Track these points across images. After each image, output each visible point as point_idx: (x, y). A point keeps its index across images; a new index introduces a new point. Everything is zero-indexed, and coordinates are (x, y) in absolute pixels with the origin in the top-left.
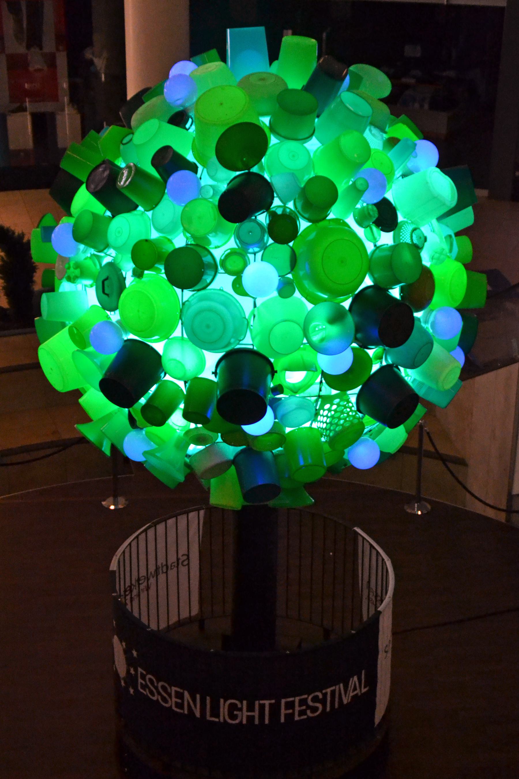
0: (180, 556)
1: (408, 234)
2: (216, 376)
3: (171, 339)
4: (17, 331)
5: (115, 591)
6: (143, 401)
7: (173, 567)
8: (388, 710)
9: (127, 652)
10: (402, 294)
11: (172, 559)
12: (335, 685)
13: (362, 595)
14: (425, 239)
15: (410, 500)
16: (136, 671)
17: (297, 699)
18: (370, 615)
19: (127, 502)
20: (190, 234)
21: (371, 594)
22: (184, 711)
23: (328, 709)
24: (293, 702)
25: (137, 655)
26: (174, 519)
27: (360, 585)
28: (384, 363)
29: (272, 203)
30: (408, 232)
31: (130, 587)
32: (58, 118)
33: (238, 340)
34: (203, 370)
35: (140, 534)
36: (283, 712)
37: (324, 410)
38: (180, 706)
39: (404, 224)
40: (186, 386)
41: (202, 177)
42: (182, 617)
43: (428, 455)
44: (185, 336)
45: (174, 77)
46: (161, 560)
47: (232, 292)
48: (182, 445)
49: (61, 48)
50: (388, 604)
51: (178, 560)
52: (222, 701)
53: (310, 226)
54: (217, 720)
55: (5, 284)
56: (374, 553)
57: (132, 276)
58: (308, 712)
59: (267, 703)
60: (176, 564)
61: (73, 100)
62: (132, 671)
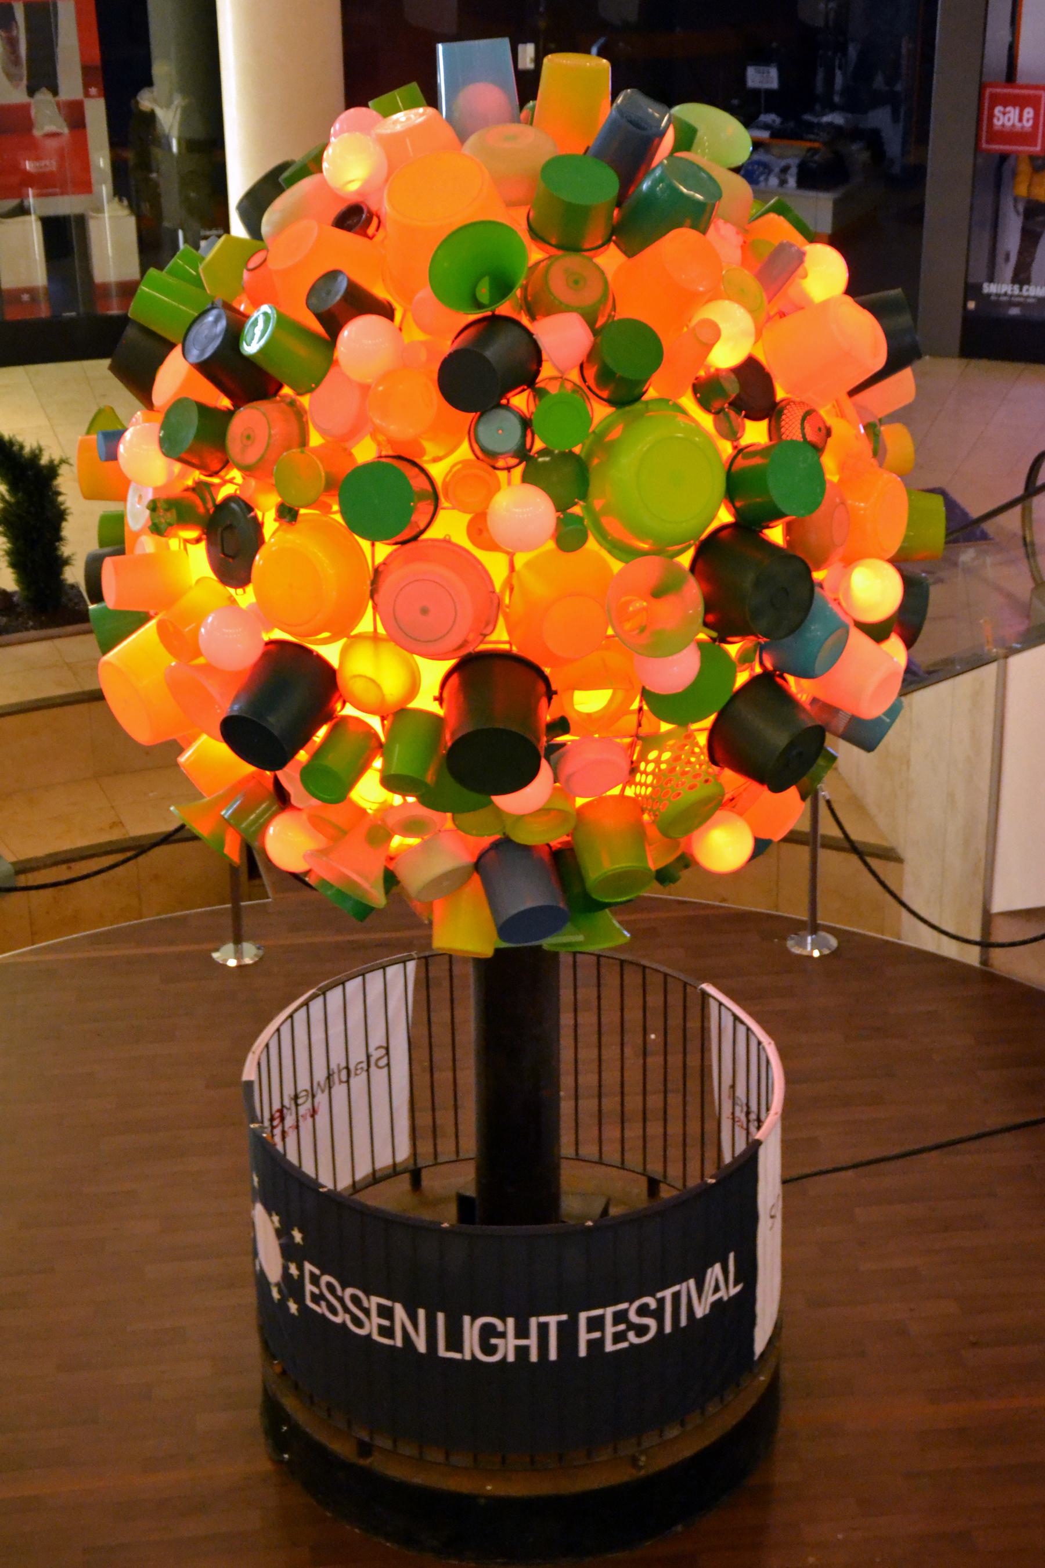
0: (371, 1050)
2: (441, 704)
3: (355, 636)
4: (33, 634)
5: (254, 1119)
7: (358, 1072)
8: (778, 1328)
9: (283, 1233)
10: (788, 537)
11: (357, 1056)
12: (680, 1282)
13: (720, 1113)
14: (828, 432)
15: (797, 928)
16: (300, 1268)
17: (609, 1312)
18: (737, 1153)
19: (261, 953)
21: (738, 1109)
23: (668, 1329)
24: (602, 1318)
25: (303, 1239)
27: (716, 1096)
28: (758, 670)
30: (797, 418)
31: (281, 1111)
32: (92, 226)
33: (481, 634)
34: (417, 693)
35: (296, 1010)
36: (584, 1337)
37: (648, 762)
38: (387, 1332)
39: (788, 404)
40: (383, 725)
41: (404, 329)
42: (379, 1165)
43: (830, 844)
44: (381, 630)
47: (467, 544)
49: (93, 91)
50: (774, 1126)
51: (368, 1057)
52: (467, 1319)
54: (457, 1356)
55: (9, 545)
56: (741, 1030)
58: (631, 1335)
59: (552, 1320)
60: (365, 1065)
61: (121, 189)
62: (293, 1270)
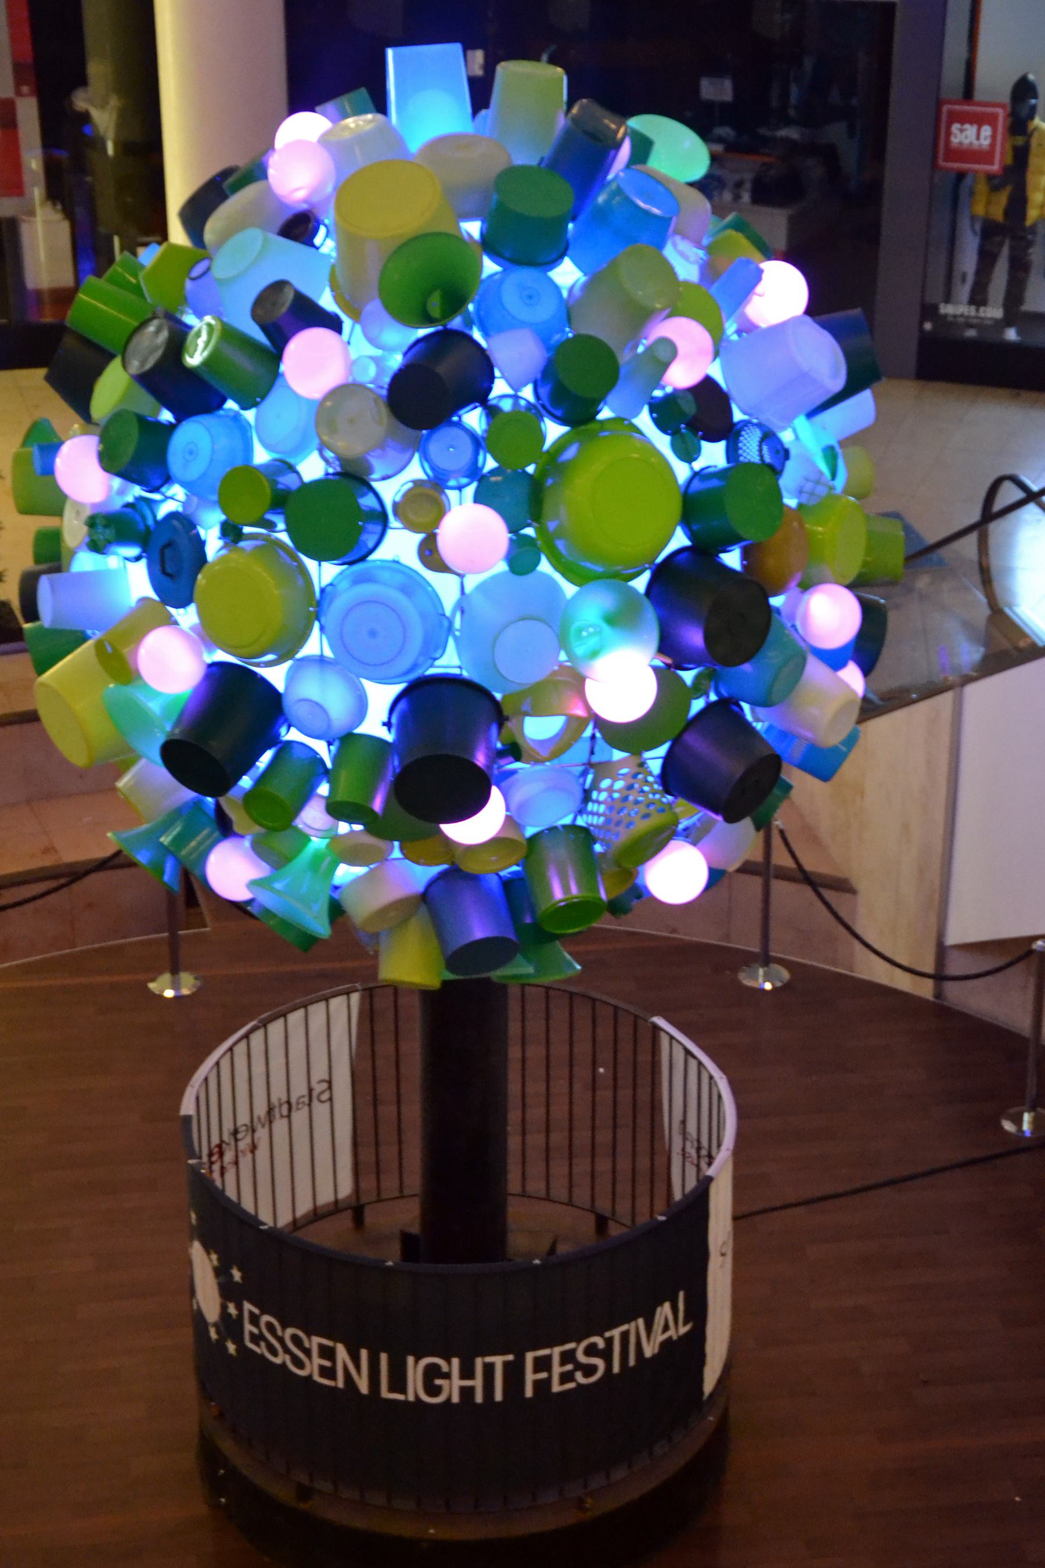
0: (314, 1084)
1: (754, 445)
2: (389, 730)
5: (193, 1155)
6: (246, 782)
8: (727, 1368)
9: (221, 1272)
11: (299, 1089)
12: (628, 1322)
15: (748, 960)
16: (240, 1308)
17: (556, 1351)
19: (198, 983)
20: (332, 452)
21: (688, 1144)
22: (336, 1383)
23: (616, 1369)
24: (548, 1359)
25: (242, 1278)
26: (301, 1013)
29: (490, 389)
31: (220, 1146)
32: (25, 229)
36: (530, 1377)
38: (329, 1373)
40: (329, 751)
41: (352, 341)
43: (783, 875)
45: (289, 146)
46: (278, 1093)
48: (323, 866)
49: (25, 89)
50: (725, 1162)
51: (310, 1090)
52: (410, 1360)
53: (567, 433)
56: (693, 1064)
57: (220, 538)
60: (306, 1100)
61: (55, 193)
62: (232, 1310)
